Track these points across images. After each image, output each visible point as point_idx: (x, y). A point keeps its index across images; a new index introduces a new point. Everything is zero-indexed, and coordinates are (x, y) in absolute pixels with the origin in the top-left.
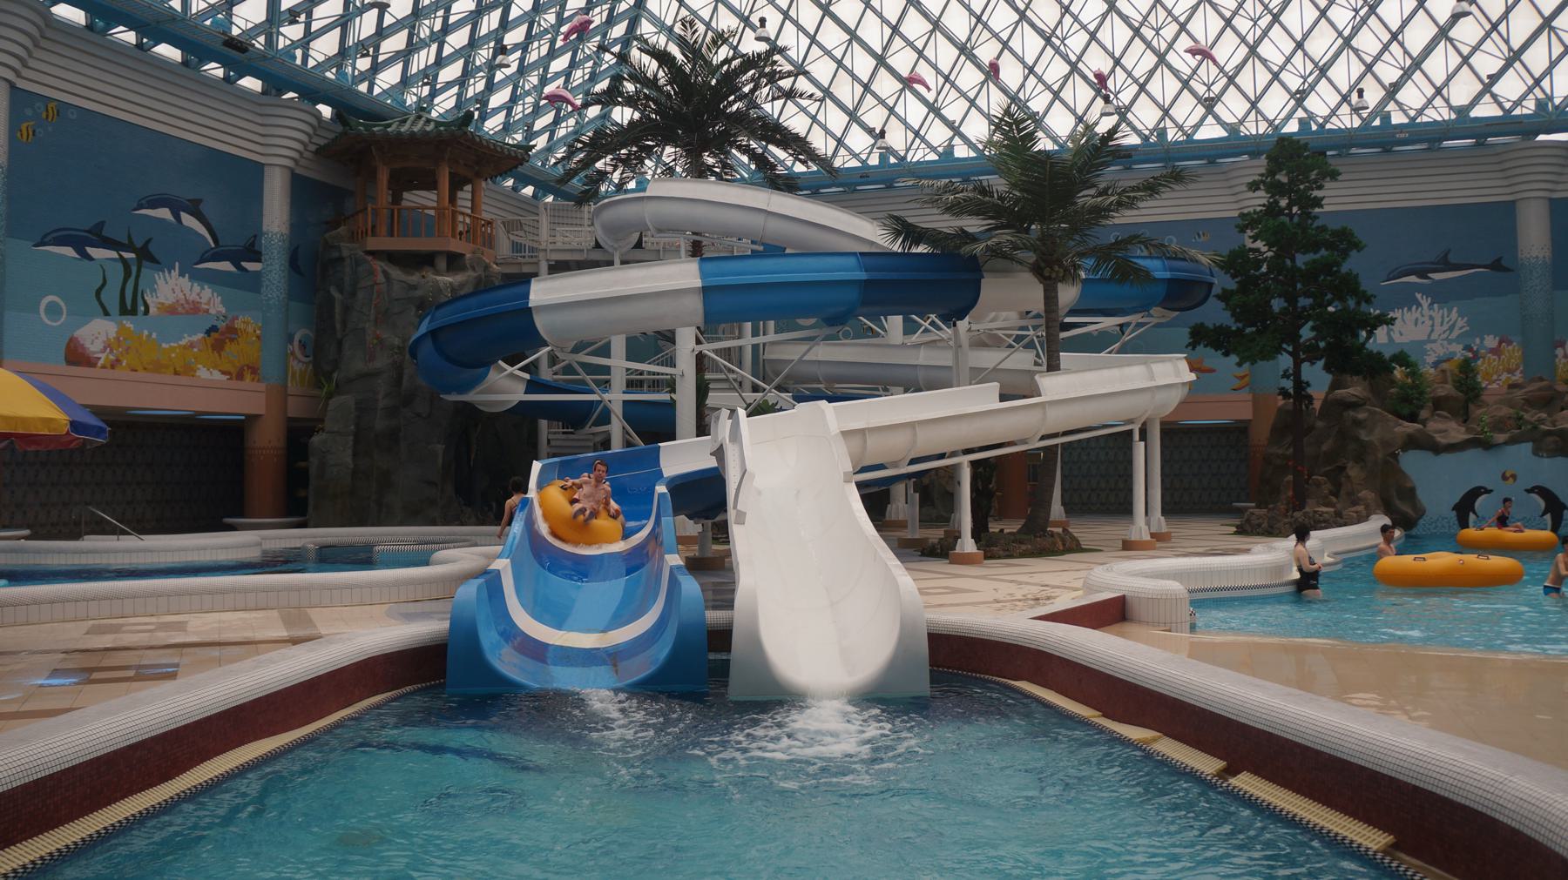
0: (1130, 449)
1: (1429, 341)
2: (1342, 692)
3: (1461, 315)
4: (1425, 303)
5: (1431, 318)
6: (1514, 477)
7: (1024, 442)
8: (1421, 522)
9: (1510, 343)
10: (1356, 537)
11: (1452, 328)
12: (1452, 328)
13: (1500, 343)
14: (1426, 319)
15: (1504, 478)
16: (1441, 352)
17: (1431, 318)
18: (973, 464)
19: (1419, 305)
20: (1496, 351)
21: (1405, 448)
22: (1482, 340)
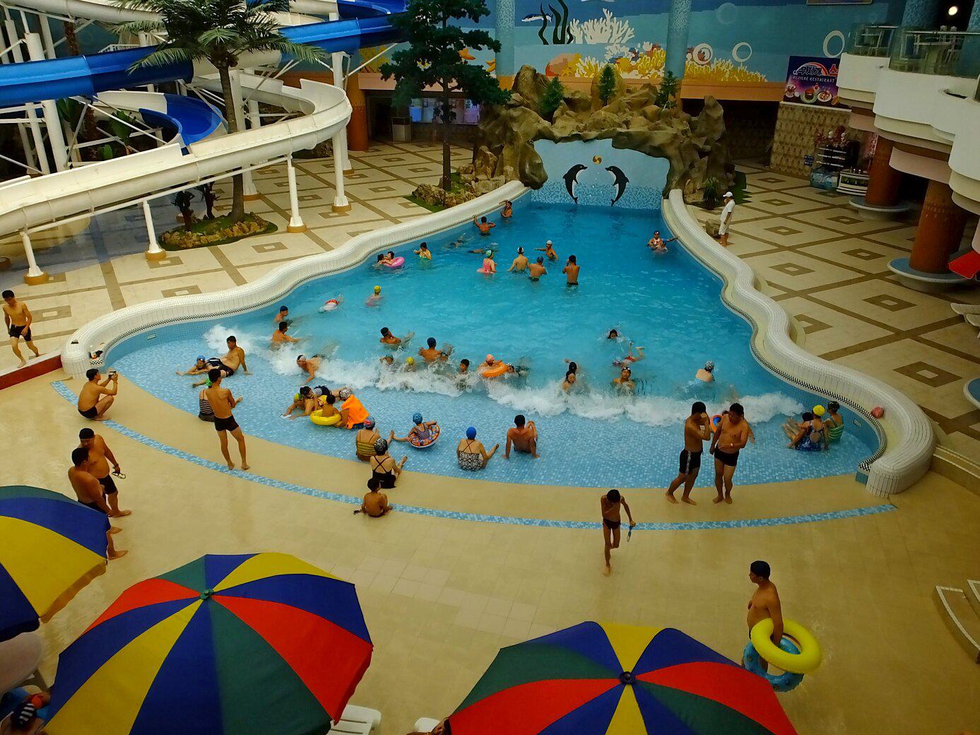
0: (286, 170)
1: (608, 44)
2: (807, 107)
3: (630, 26)
4: (608, 16)
5: (611, 27)
6: (600, 159)
7: (192, 182)
8: (545, 184)
9: (659, 48)
10: (443, 220)
11: (623, 36)
12: (623, 36)
13: (653, 48)
14: (608, 28)
15: (594, 160)
16: (615, 52)
17: (611, 27)
18: (149, 202)
19: (605, 18)
20: (650, 54)
21: (535, 139)
22: (642, 45)
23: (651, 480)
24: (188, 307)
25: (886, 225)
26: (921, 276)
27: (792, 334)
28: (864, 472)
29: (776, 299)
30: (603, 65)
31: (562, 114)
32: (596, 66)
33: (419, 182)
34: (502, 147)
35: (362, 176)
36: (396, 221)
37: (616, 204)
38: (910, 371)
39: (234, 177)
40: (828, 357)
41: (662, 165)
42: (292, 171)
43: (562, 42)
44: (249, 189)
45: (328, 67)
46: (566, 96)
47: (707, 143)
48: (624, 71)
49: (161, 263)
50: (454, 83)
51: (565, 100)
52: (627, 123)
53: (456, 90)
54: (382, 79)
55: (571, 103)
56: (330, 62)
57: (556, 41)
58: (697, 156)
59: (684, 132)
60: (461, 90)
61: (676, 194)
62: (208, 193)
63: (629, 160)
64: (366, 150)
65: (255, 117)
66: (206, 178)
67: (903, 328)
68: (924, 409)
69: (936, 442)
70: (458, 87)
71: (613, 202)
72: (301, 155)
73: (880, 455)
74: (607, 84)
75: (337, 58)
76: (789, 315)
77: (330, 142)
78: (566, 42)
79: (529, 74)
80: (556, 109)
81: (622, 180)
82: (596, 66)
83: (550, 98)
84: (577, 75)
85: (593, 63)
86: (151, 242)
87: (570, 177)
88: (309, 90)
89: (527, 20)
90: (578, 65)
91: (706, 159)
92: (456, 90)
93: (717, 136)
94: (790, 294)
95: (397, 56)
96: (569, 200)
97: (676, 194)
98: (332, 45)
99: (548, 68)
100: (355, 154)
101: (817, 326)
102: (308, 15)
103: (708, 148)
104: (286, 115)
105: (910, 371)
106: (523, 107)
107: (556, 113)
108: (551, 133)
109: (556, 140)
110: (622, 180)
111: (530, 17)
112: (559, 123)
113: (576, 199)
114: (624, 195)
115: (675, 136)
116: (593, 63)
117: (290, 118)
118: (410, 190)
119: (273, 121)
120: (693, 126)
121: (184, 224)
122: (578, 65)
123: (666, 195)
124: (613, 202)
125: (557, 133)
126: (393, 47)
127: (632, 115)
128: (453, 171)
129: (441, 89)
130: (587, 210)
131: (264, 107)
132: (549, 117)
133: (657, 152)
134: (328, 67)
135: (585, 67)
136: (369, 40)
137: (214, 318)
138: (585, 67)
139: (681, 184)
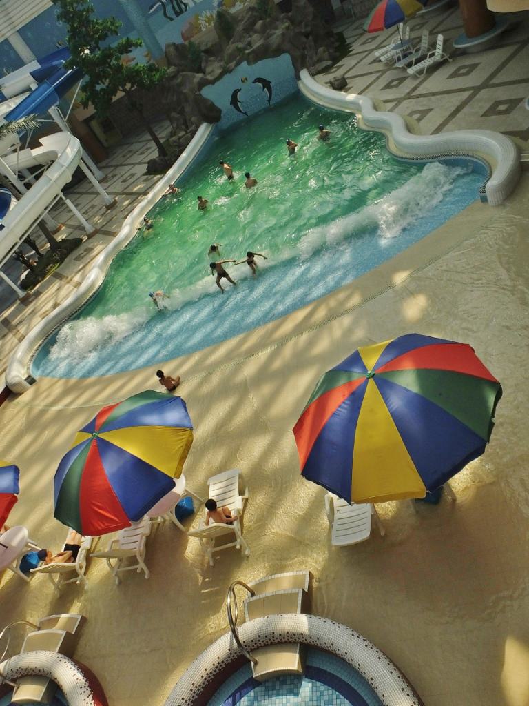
15: (243, 81)
23: (362, 269)
24: (59, 314)
25: (440, 19)
26: (471, 42)
27: (409, 129)
28: (483, 194)
29: (391, 110)
30: (215, 12)
31: (207, 63)
32: (212, 16)
33: (147, 160)
34: (183, 107)
35: (113, 176)
36: (145, 193)
37: (272, 103)
38: (492, 111)
39: (38, 224)
40: (438, 130)
41: (285, 59)
42: (68, 202)
43: (181, 12)
44: (51, 224)
45: (51, 121)
46: (203, 48)
47: (306, 26)
48: (230, 7)
49: (30, 300)
50: (128, 86)
51: (203, 52)
52: (249, 44)
53: (134, 88)
54: (84, 108)
55: (208, 52)
56: (50, 117)
57: (178, 14)
58: (304, 39)
59: (288, 28)
60: (135, 87)
61: (304, 74)
62: (29, 242)
63: (265, 68)
64: (107, 157)
65: (30, 178)
66: (23, 235)
67: (478, 84)
68: (503, 133)
69: (520, 151)
70: (132, 86)
71: (269, 101)
72: (67, 190)
73: (490, 177)
74: (225, 24)
75: (53, 111)
76: (402, 116)
77: (78, 167)
78: (184, 10)
79: (172, 49)
80: (201, 62)
81: (266, 84)
82: (212, 16)
83: (189, 57)
84: (204, 29)
85: (208, 15)
86: (334, 91)
87: (234, 101)
88: (48, 143)
89: (151, 11)
90: (200, 22)
91: (311, 38)
92: (134, 88)
93: (310, 18)
94: (399, 101)
95: (84, 89)
96: (242, 117)
97: (304, 74)
98: (47, 103)
99: (183, 35)
100: (103, 164)
101: (424, 113)
102: (15, 96)
103: (309, 29)
104: (45, 168)
105: (492, 111)
106: (181, 73)
107: (203, 66)
108: (207, 80)
109: (213, 82)
110: (266, 84)
111: (152, 7)
112: (208, 70)
113: (245, 113)
114: (273, 92)
115: (283, 35)
116: (208, 15)
117: (48, 168)
118: (144, 168)
119: (41, 174)
120: (292, 21)
121: (29, 270)
122: (200, 22)
123: (298, 78)
124: (269, 101)
125: (210, 78)
126: (81, 83)
127: (250, 36)
128: (162, 141)
129: (123, 94)
130: (257, 115)
131: (32, 170)
132: (200, 70)
133: (278, 52)
134: (51, 121)
135: (205, 21)
136: (63, 89)
137: (404, 160)
138: (205, 21)
139: (303, 66)
